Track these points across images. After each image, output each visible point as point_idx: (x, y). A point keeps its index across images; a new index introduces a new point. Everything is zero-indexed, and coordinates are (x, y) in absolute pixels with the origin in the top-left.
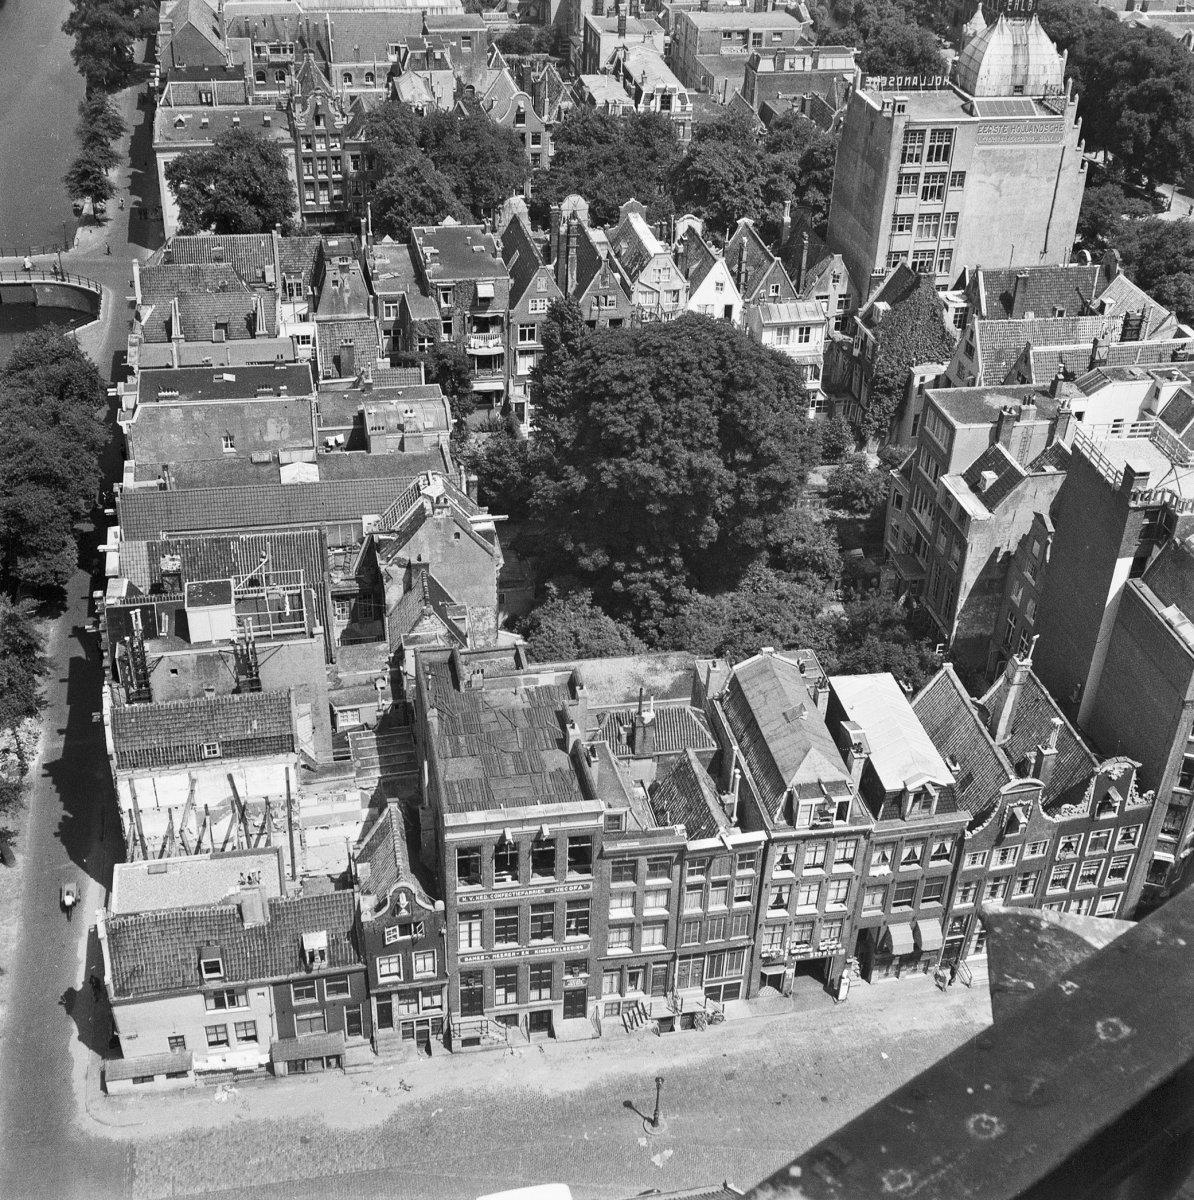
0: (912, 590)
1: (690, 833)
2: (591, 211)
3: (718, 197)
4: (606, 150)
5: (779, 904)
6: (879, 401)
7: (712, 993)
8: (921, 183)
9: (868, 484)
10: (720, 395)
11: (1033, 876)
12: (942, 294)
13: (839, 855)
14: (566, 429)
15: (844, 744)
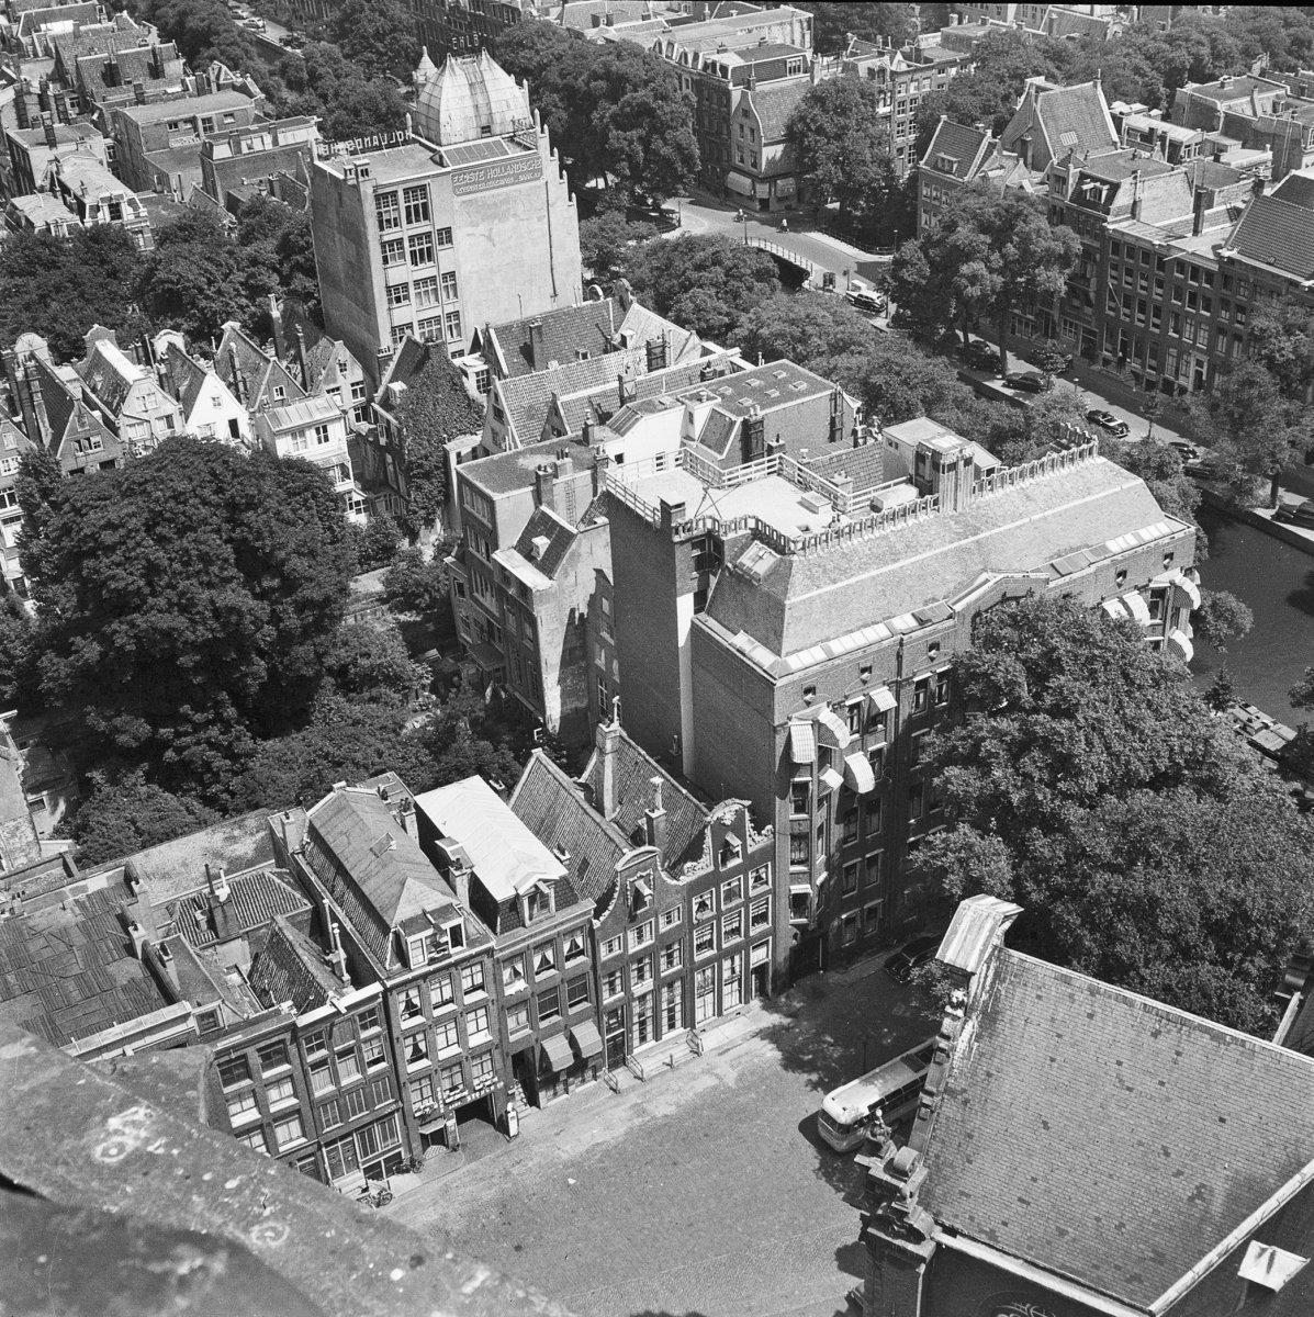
0: (498, 680)
1: (298, 1005)
2: (51, 347)
3: (194, 305)
4: (55, 277)
5: (418, 1055)
6: (419, 488)
7: (373, 1172)
8: (408, 250)
9: (428, 579)
10: (228, 521)
11: (676, 946)
12: (457, 362)
13: (466, 984)
14: (65, 598)
15: (441, 862)
